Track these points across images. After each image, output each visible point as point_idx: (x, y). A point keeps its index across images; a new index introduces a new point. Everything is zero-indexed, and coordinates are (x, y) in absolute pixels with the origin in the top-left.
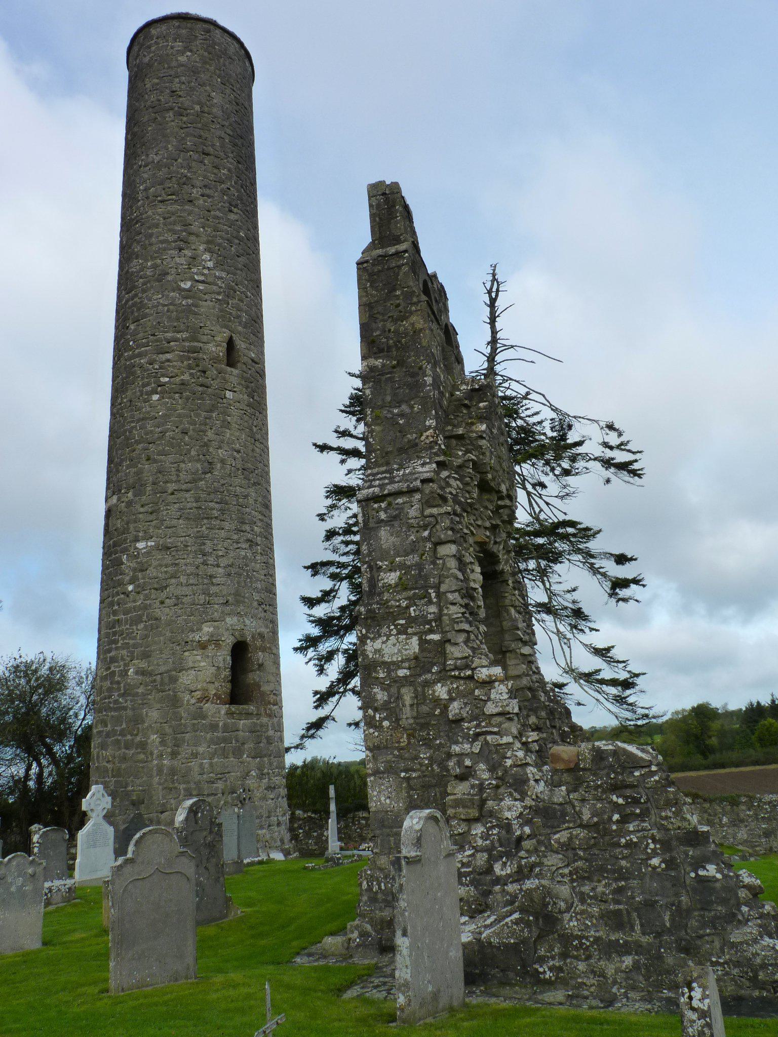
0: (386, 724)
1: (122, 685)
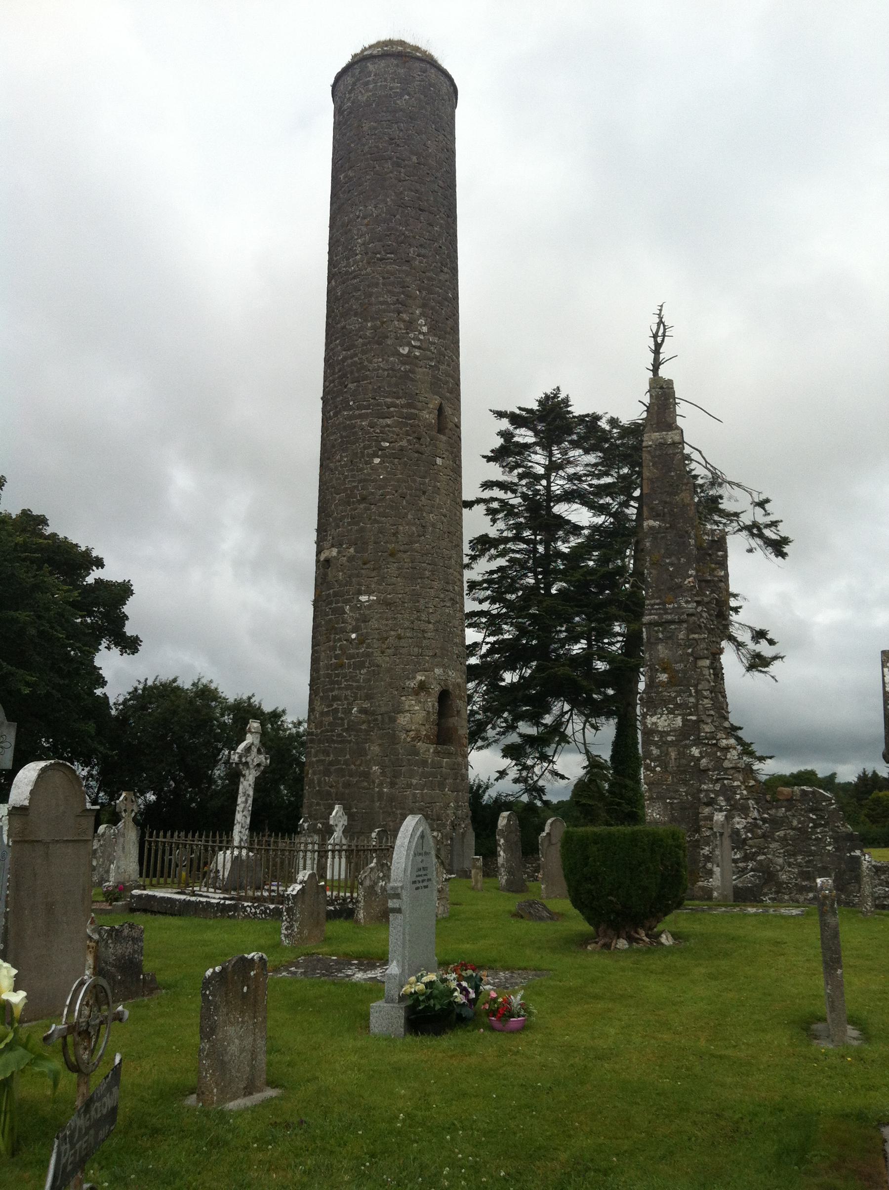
0: (658, 769)
1: (346, 721)
